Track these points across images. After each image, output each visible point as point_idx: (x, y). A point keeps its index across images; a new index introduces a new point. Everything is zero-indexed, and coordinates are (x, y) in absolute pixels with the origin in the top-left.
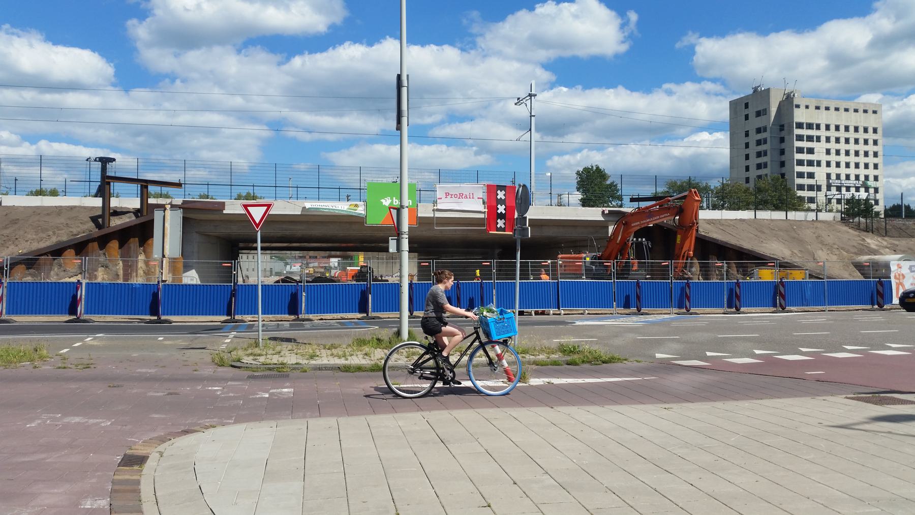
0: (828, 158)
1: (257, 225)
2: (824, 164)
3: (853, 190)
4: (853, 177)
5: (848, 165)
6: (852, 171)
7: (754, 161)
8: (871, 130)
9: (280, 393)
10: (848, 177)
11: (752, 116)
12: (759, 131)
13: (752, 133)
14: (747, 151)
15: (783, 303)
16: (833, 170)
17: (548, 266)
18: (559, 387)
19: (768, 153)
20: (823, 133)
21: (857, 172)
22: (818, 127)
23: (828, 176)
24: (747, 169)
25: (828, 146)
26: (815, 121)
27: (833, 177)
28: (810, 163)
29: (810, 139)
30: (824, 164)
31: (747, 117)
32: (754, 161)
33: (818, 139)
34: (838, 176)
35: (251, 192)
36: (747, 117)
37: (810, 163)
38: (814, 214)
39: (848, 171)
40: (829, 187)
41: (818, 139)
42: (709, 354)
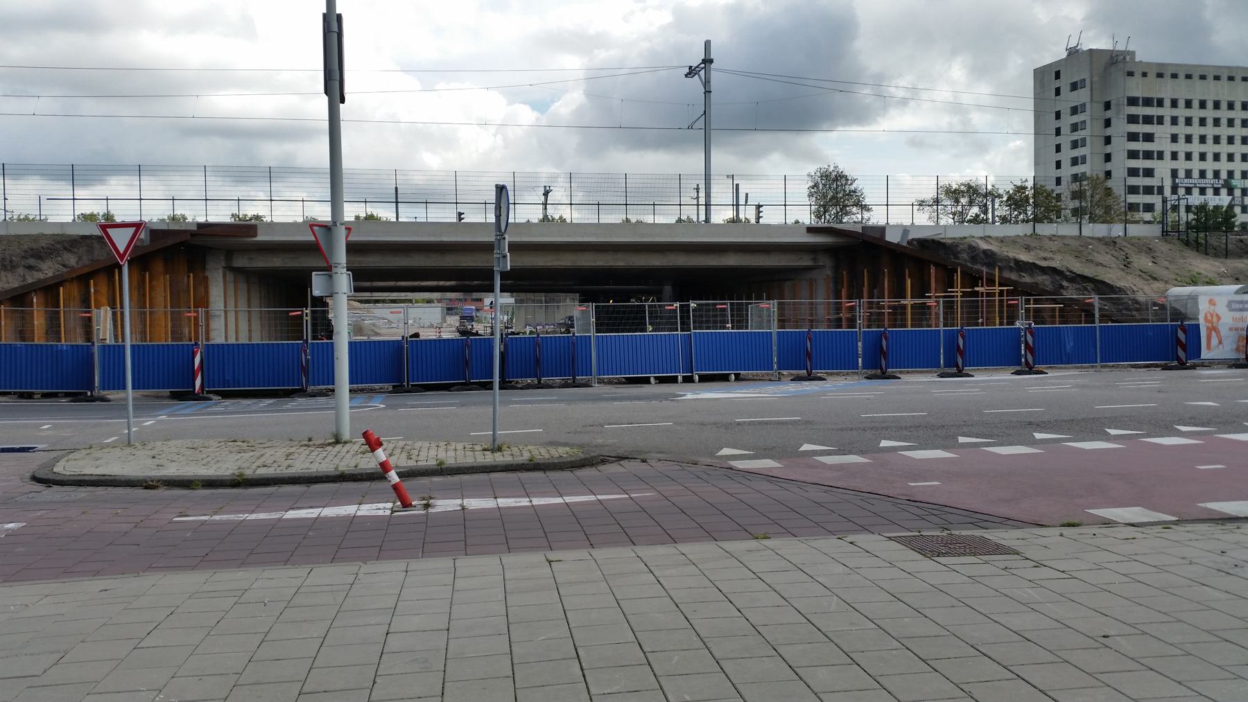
0: (1174, 147)
2: (1168, 156)
3: (1210, 192)
4: (1210, 175)
5: (1189, 156)
6: (1210, 166)
7: (1067, 154)
8: (1224, 105)
10: (1203, 174)
11: (1065, 89)
12: (1074, 111)
16: (1181, 165)
20: (1167, 112)
21: (1217, 166)
22: (1160, 103)
23: (1174, 173)
25: (1175, 130)
26: (1155, 95)
27: (1182, 174)
28: (1148, 155)
29: (1148, 120)
30: (1168, 156)
31: (1058, 92)
32: (1067, 154)
33: (1160, 120)
34: (1189, 174)
36: (1058, 92)
37: (1148, 155)
39: (1203, 165)
40: (1174, 189)
41: (1160, 120)
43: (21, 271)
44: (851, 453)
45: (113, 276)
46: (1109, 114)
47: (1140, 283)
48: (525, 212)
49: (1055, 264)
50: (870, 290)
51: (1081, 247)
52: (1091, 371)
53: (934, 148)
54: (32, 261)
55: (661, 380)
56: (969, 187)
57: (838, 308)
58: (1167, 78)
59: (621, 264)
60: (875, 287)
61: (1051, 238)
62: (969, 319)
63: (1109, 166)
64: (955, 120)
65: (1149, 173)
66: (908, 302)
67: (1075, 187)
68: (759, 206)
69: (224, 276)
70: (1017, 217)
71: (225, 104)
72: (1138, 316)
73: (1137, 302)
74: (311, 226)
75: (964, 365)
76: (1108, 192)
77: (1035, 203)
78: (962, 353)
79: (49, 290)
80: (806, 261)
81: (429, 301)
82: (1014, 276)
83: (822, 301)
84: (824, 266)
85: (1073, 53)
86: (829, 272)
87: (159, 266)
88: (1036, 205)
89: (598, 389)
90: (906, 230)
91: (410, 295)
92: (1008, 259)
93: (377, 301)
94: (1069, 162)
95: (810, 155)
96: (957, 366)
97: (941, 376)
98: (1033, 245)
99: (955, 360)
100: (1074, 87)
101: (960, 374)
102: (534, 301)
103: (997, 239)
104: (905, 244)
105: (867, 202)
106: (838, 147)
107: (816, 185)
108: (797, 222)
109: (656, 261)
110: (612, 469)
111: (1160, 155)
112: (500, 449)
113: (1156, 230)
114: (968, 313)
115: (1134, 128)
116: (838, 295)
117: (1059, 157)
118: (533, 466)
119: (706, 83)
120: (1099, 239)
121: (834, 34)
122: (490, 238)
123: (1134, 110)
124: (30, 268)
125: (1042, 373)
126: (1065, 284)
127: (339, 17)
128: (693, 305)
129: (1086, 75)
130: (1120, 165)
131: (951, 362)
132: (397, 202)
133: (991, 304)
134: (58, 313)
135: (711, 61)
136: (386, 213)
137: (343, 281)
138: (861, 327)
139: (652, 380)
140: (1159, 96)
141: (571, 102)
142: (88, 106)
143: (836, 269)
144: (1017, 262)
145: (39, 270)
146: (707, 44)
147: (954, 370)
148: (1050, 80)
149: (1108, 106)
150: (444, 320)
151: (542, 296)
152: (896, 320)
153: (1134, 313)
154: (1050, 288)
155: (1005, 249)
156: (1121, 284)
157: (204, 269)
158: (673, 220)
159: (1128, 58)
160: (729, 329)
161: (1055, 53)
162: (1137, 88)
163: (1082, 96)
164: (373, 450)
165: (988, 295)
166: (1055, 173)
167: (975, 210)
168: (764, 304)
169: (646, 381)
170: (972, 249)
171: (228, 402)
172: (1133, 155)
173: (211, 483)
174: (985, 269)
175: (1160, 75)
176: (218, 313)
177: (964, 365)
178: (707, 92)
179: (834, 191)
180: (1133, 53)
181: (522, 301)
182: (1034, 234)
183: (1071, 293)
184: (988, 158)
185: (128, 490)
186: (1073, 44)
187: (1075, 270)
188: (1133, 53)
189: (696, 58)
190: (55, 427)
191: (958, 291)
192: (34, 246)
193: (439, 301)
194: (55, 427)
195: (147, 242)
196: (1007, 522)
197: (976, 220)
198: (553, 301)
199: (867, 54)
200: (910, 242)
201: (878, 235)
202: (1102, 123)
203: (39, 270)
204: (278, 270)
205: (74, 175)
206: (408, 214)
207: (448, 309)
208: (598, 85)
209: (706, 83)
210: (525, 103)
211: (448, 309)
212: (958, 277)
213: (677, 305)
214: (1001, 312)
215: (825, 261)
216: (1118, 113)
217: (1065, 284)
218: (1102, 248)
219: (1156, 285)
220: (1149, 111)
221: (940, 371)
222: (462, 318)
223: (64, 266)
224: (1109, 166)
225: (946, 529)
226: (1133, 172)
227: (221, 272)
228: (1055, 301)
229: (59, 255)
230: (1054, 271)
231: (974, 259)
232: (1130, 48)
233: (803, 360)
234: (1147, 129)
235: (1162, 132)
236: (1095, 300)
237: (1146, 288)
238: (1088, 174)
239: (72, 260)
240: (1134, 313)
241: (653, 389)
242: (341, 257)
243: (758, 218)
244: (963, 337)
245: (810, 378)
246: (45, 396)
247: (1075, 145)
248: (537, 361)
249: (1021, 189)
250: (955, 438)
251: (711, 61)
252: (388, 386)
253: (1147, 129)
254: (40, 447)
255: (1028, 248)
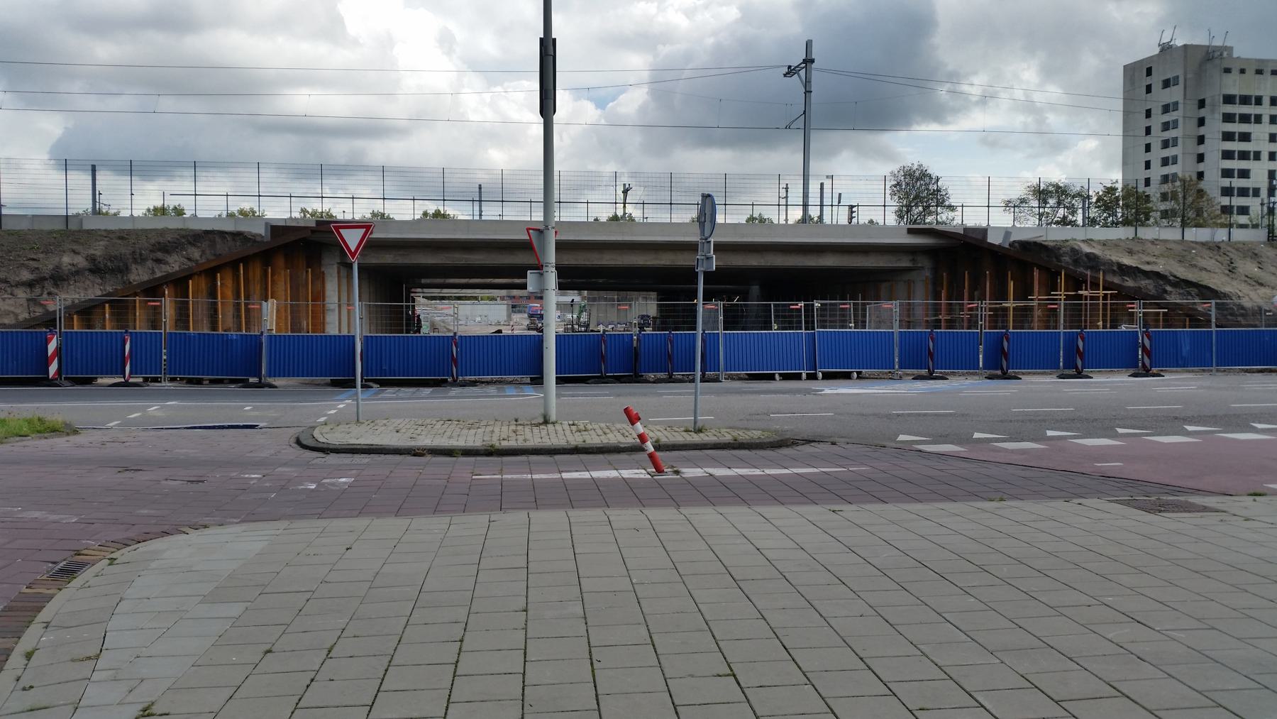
1: (353, 255)
2: (1265, 156)
7: (1157, 154)
9: (333, 484)
11: (1157, 87)
12: (1166, 109)
13: (1156, 111)
14: (1148, 140)
15: (1147, 361)
17: (800, 310)
18: (722, 482)
19: (1180, 141)
22: (1259, 101)
24: (1148, 165)
28: (1244, 156)
29: (1245, 119)
30: (1265, 156)
32: (1157, 154)
33: (1258, 119)
35: (441, 209)
36: (1149, 89)
37: (1244, 156)
38: (1225, 231)
41: (1258, 119)
42: (1050, 433)
43: (150, 263)
44: (1022, 440)
45: (238, 270)
46: (1203, 112)
47: (1245, 289)
48: (730, 217)
49: (1159, 268)
50: (972, 292)
51: (1184, 252)
52: (1206, 375)
53: (1016, 147)
54: (159, 255)
55: (785, 377)
56: (1057, 187)
57: (937, 309)
58: (1267, 75)
59: (663, 262)
60: (976, 289)
61: (1154, 242)
62: (1072, 321)
63: (1201, 167)
64: (1030, 119)
65: (1244, 174)
66: (1010, 304)
67: (1166, 188)
68: (851, 207)
69: (339, 273)
70: (1106, 219)
71: (304, 102)
72: (1243, 322)
73: (1243, 308)
74: (528, 230)
75: (1083, 367)
76: (1201, 193)
77: (1129, 205)
78: (1082, 356)
79: (179, 283)
80: (905, 263)
81: (493, 299)
82: (1116, 280)
83: (920, 301)
84: (923, 268)
85: (1166, 49)
86: (927, 273)
87: (280, 261)
88: (1126, 206)
89: (726, 384)
90: (1007, 232)
91: (477, 292)
92: (1111, 263)
93: (443, 298)
94: (1159, 162)
95: (884, 154)
96: (1077, 368)
97: (1060, 377)
98: (1136, 249)
99: (1075, 363)
100: (1166, 84)
101: (1079, 375)
102: (606, 299)
103: (1099, 242)
104: (1007, 246)
105: (953, 201)
106: (913, 146)
107: (898, 184)
108: (871, 222)
109: (754, 261)
110: (807, 449)
111: (1257, 156)
112: (700, 431)
113: (1261, 234)
114: (1072, 316)
115: (1230, 127)
116: (937, 296)
117: (1148, 156)
118: (736, 445)
119: (807, 83)
120: (1203, 244)
121: (916, 27)
122: (694, 237)
123: (1229, 109)
124: (158, 261)
125: (1159, 375)
126: (1169, 288)
127: (554, 40)
128: (817, 304)
129: (1179, 72)
130: (1214, 165)
131: (1070, 364)
132: (480, 201)
133: (1094, 308)
134: (216, 304)
135: (812, 61)
136: (460, 212)
137: (552, 278)
138: (984, 328)
139: (777, 377)
140: (1258, 93)
141: (633, 102)
142: (167, 103)
143: (935, 270)
144: (1120, 266)
145: (166, 263)
146: (809, 45)
147: (1073, 372)
148: (1141, 76)
149: (1202, 104)
150: (509, 317)
151: (615, 295)
152: (996, 322)
153: (1240, 319)
154: (1153, 292)
155: (1107, 253)
156: (1227, 289)
157: (320, 265)
158: (742, 219)
159: (1225, 54)
160: (851, 328)
161: (1147, 49)
162: (1234, 85)
163: (1175, 94)
164: (633, 424)
165: (1092, 298)
166: (1144, 174)
167: (1061, 212)
168: (886, 305)
169: (771, 377)
170: (1075, 252)
171: (390, 391)
172: (1227, 155)
173: (468, 452)
174: (1089, 273)
175: (1259, 72)
176: (332, 307)
177: (1083, 367)
178: (808, 92)
179: (918, 190)
180: (1231, 49)
181: (594, 300)
182: (1136, 238)
183: (1174, 298)
184: (1060, 158)
185: (398, 458)
186: (1165, 40)
187: (1179, 275)
188: (1231, 49)
189: (797, 59)
190: (255, 409)
191: (1061, 294)
192: (161, 240)
193: (502, 298)
194: (255, 409)
195: (268, 238)
196: (1198, 491)
197: (1064, 222)
198: (625, 299)
199: (944, 49)
200: (1012, 244)
201: (979, 237)
202: (1195, 122)
203: (166, 263)
204: (402, 268)
205: (132, 169)
206: (491, 212)
207: (514, 307)
208: (662, 83)
209: (807, 83)
210: (590, 99)
211: (514, 307)
212: (1062, 281)
213: (802, 304)
214: (1104, 315)
215: (925, 262)
216: (1213, 112)
217: (1169, 288)
218: (1206, 253)
219: (1262, 291)
220: (1245, 109)
221: (1060, 372)
222: (531, 316)
223: (189, 259)
224: (1201, 167)
225: (1157, 494)
226: (1227, 173)
227: (335, 267)
228: (1159, 306)
229: (183, 249)
230: (1157, 275)
231: (1076, 262)
232: (1228, 44)
233: (924, 359)
234: (1244, 128)
235: (1261, 132)
236: (1201, 305)
237: (1252, 294)
238: (1180, 175)
239: (196, 254)
240: (1240, 319)
241: (778, 384)
242: (551, 257)
243: (851, 218)
244: (1083, 339)
245: (931, 377)
246: (213, 382)
247: (1166, 144)
248: (670, 357)
249: (1110, 190)
250: (1112, 428)
251: (812, 61)
252: (527, 379)
253: (1244, 128)
254: (261, 425)
255: (1131, 252)
